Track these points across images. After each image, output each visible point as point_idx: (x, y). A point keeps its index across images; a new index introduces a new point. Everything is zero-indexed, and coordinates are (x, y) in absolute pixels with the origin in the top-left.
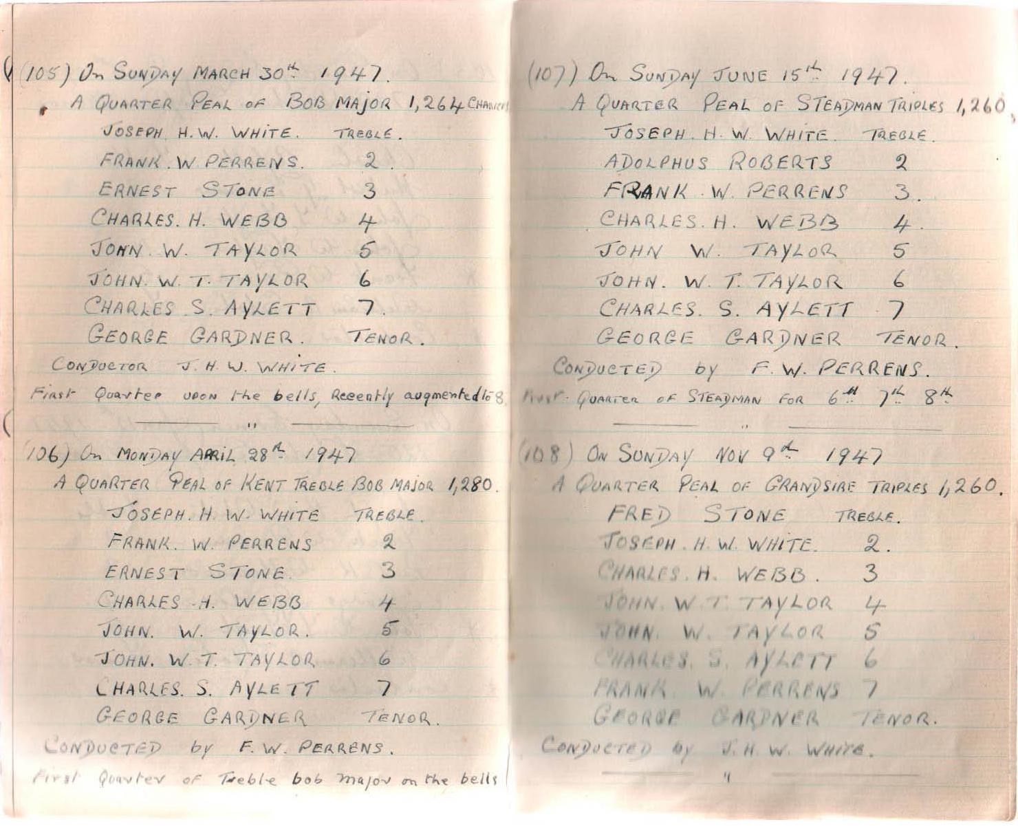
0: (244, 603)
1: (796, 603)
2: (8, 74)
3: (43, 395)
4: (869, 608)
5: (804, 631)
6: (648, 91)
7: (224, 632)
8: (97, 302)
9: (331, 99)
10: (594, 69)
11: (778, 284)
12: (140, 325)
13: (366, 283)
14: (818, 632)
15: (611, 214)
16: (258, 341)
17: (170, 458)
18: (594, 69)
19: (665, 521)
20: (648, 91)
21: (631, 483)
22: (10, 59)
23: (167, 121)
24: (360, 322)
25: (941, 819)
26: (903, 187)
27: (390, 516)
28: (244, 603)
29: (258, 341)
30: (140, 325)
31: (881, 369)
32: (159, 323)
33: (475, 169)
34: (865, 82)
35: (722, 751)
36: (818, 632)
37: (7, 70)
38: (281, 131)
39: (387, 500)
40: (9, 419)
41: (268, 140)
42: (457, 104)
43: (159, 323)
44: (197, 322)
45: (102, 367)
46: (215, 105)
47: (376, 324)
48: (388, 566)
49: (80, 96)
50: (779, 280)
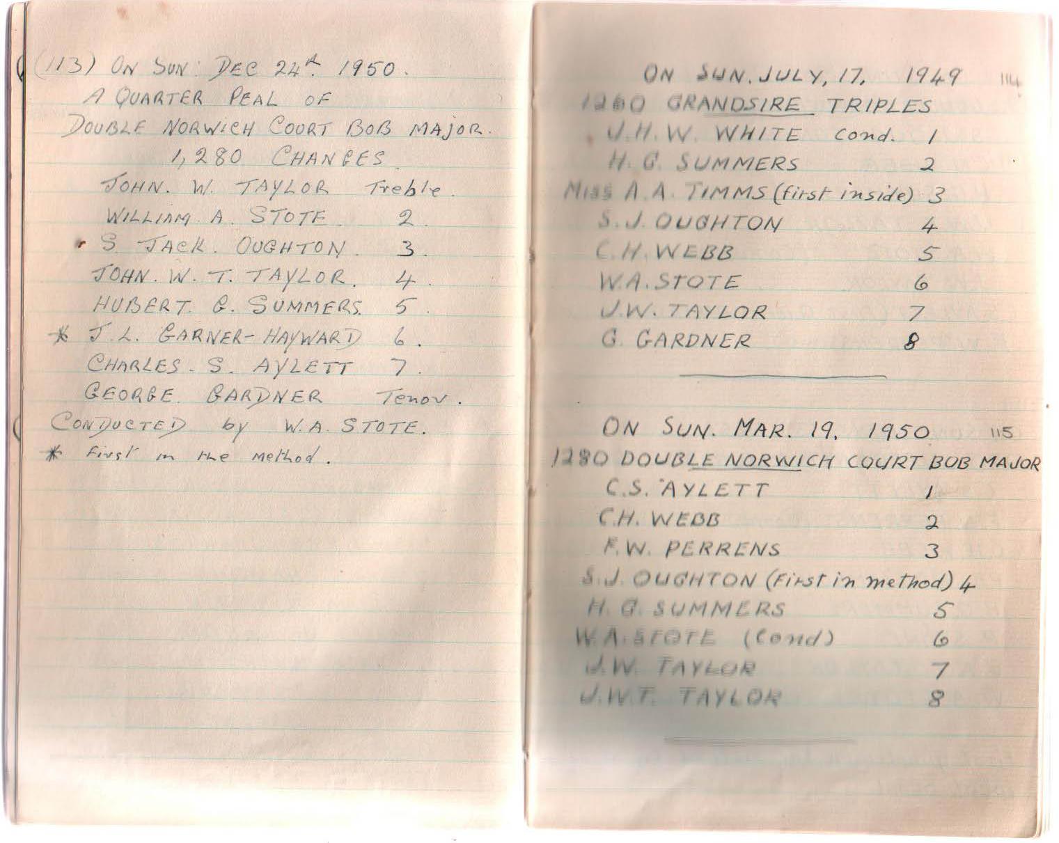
1: (703, 493)
2: (20, 74)
7: (727, 313)
8: (66, 419)
10: (745, 315)
11: (323, 341)
12: (144, 381)
14: (707, 637)
16: (213, 341)
18: (745, 315)
22: (18, 422)
27: (112, 128)
29: (213, 341)
30: (144, 381)
32: (163, 381)
35: (625, 224)
36: (707, 637)
41: (749, 320)
43: (163, 381)
44: (214, 380)
49: (762, 424)
50: (323, 337)
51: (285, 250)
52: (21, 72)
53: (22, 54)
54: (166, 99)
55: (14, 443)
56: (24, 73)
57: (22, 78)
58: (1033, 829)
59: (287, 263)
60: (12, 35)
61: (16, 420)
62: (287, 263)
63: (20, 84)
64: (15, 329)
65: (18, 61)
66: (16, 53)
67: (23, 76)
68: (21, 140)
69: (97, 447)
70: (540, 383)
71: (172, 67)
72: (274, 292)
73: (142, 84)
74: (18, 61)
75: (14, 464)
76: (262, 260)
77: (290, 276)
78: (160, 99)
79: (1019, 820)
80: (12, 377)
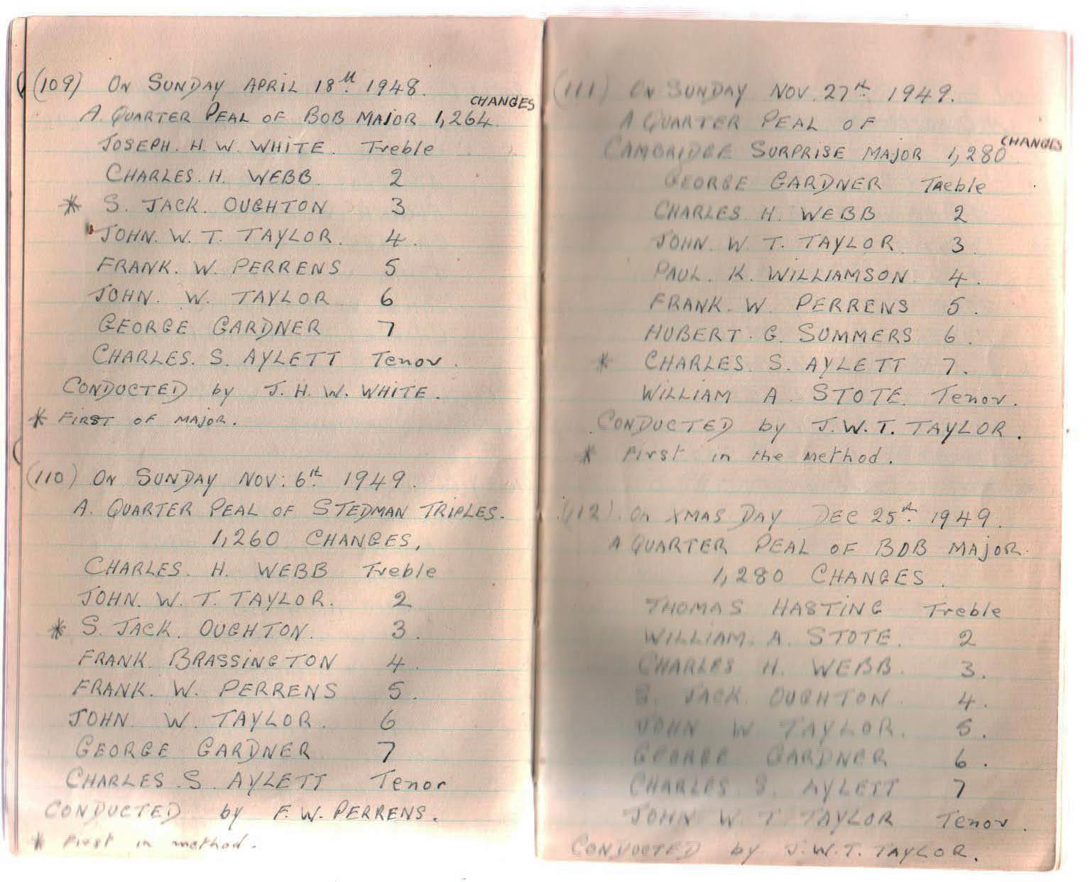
0: (175, 724)
2: (21, 90)
3: (72, 420)
4: (849, 430)
5: (836, 548)
6: (683, 108)
9: (351, 114)
13: (389, 302)
15: (106, 347)
17: (205, 482)
19: (730, 428)
20: (683, 108)
21: (735, 331)
22: (22, 76)
23: (185, 135)
24: (384, 344)
25: (1004, 870)
26: (398, 201)
28: (175, 724)
31: (861, 307)
33: (504, 188)
34: (155, 758)
37: (20, 86)
38: (311, 145)
39: (393, 558)
40: (18, 446)
42: (484, 120)
45: (121, 390)
46: (231, 118)
47: (398, 348)
48: (400, 624)
51: (217, 572)
52: (21, 89)
53: (22, 70)
54: (155, 118)
55: (15, 467)
56: (24, 88)
57: (23, 94)
58: (1050, 864)
59: (276, 223)
60: (12, 51)
61: (16, 443)
62: (276, 223)
63: (21, 101)
64: (15, 326)
65: (19, 77)
66: (17, 69)
67: (23, 92)
68: (21, 280)
69: (108, 210)
70: (551, 222)
71: (127, 508)
72: (263, 252)
73: (138, 102)
74: (19, 77)
75: (14, 488)
76: (249, 220)
77: (282, 234)
78: (150, 118)
79: (1039, 855)
80: (12, 306)
